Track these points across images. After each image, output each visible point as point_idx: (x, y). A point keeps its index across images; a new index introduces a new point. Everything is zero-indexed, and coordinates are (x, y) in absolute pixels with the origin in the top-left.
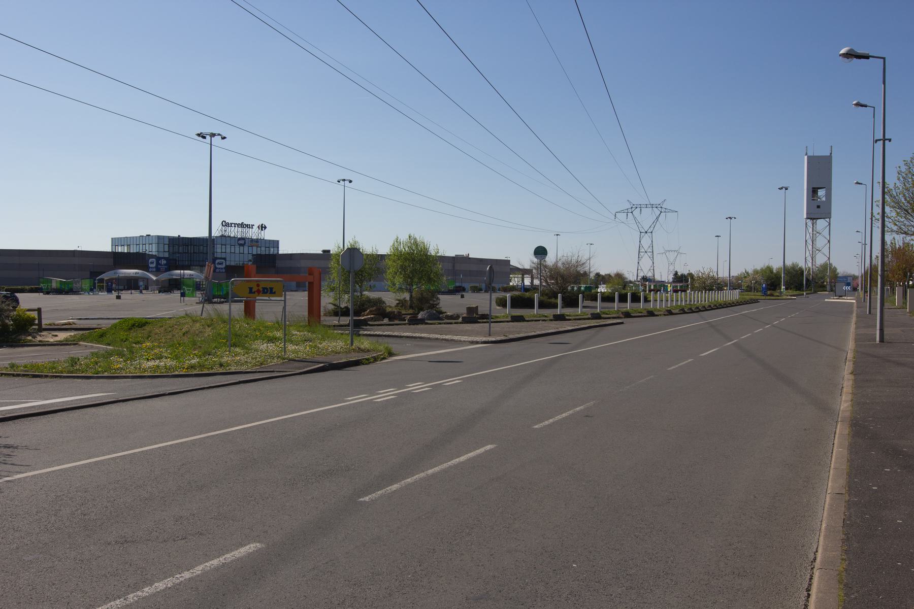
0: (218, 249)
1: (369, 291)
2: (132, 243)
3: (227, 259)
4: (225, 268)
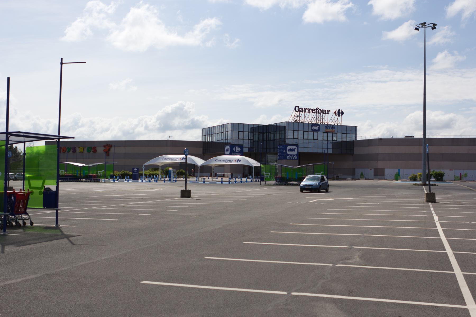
0: (290, 134)
1: (250, 167)
2: (216, 134)
3: (300, 146)
4: (296, 155)
